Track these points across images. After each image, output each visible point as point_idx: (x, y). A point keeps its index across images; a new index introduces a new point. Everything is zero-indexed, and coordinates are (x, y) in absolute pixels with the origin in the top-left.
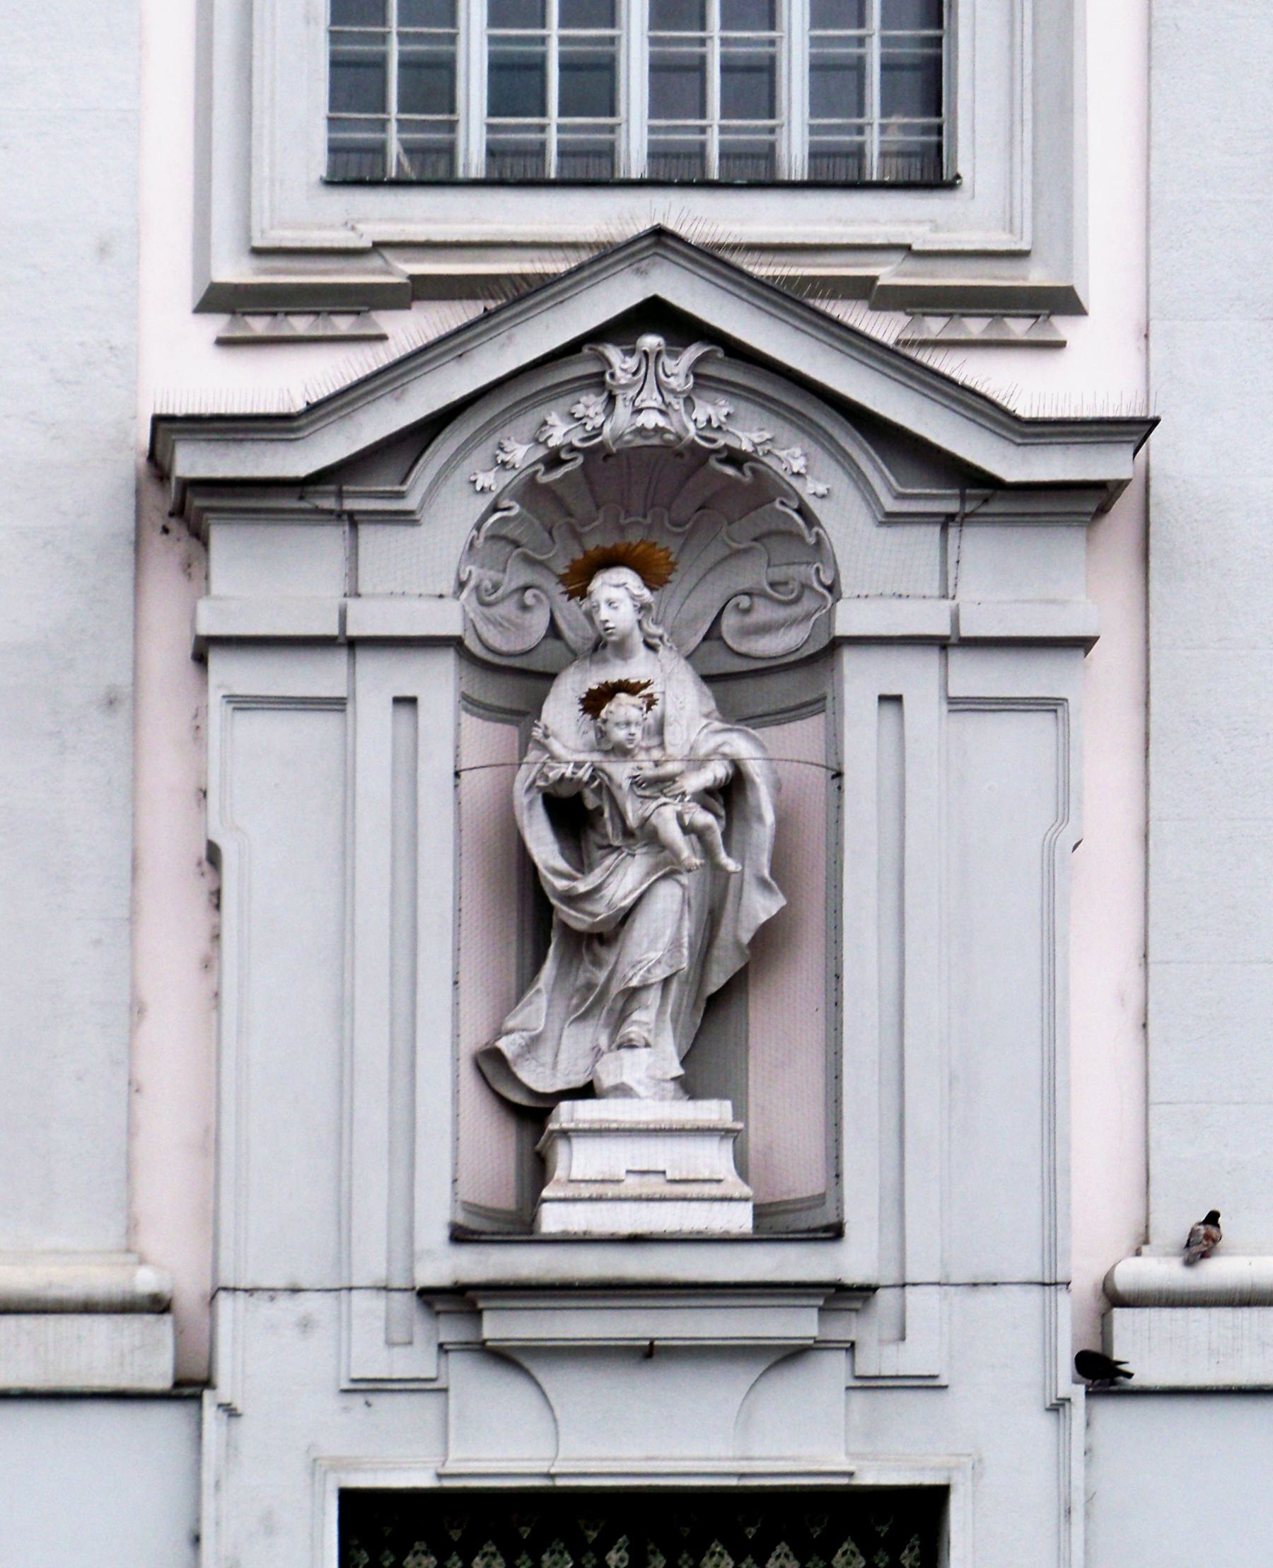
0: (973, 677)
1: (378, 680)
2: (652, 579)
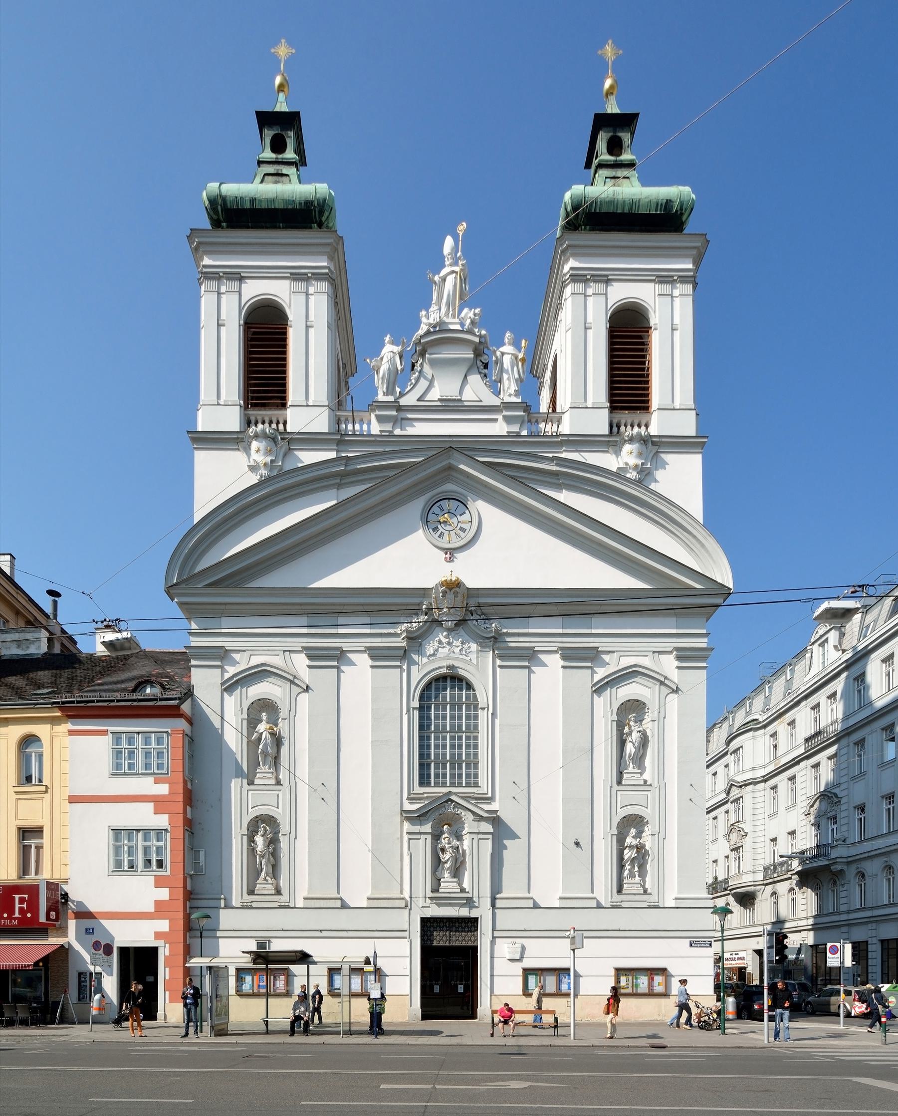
0: (481, 836)
1: (424, 837)
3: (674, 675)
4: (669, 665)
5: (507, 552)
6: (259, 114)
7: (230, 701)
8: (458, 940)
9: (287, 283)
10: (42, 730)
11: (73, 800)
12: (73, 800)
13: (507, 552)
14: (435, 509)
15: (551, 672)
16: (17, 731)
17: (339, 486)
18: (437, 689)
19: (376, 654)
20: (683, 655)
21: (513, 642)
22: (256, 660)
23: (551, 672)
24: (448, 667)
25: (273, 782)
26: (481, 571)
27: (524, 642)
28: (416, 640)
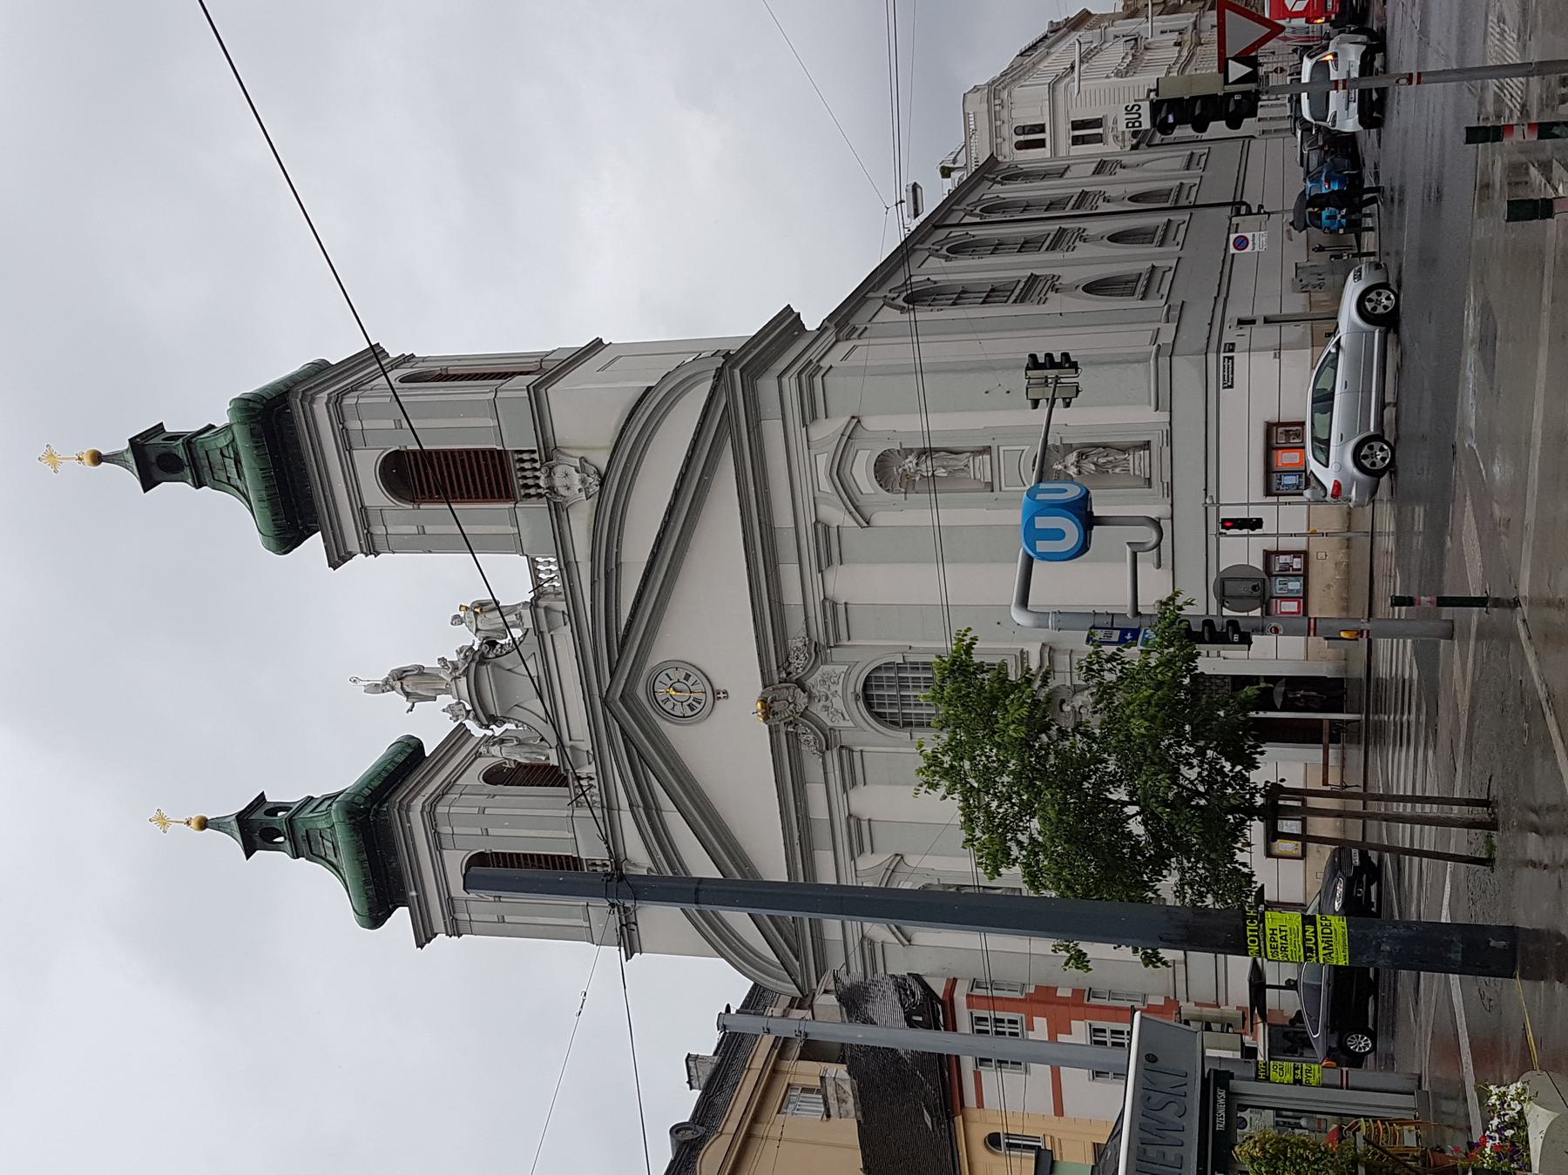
2: (1063, 701)
3: (837, 424)
4: (828, 430)
5: (711, 626)
6: (334, 565)
7: (879, 519)
8: (1140, 289)
9: (445, 852)
10: (979, 1132)
11: (1059, 1110)
12: (1059, 1110)
13: (711, 626)
14: (668, 707)
15: (845, 583)
16: (982, 1155)
17: (659, 810)
18: (881, 705)
19: (850, 780)
20: (810, 415)
21: (818, 632)
22: (825, 485)
23: (845, 583)
24: (857, 699)
25: (987, 457)
26: (737, 666)
27: (816, 611)
28: (827, 740)
